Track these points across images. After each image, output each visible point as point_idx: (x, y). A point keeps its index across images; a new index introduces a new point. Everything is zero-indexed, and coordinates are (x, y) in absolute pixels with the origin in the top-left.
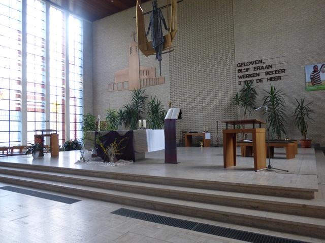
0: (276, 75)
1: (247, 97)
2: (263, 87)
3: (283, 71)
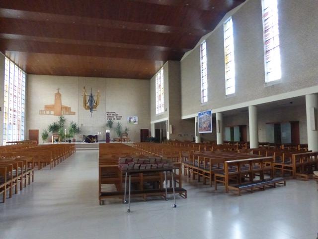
0: (119, 118)
1: (110, 124)
2: (116, 122)
3: (121, 117)
